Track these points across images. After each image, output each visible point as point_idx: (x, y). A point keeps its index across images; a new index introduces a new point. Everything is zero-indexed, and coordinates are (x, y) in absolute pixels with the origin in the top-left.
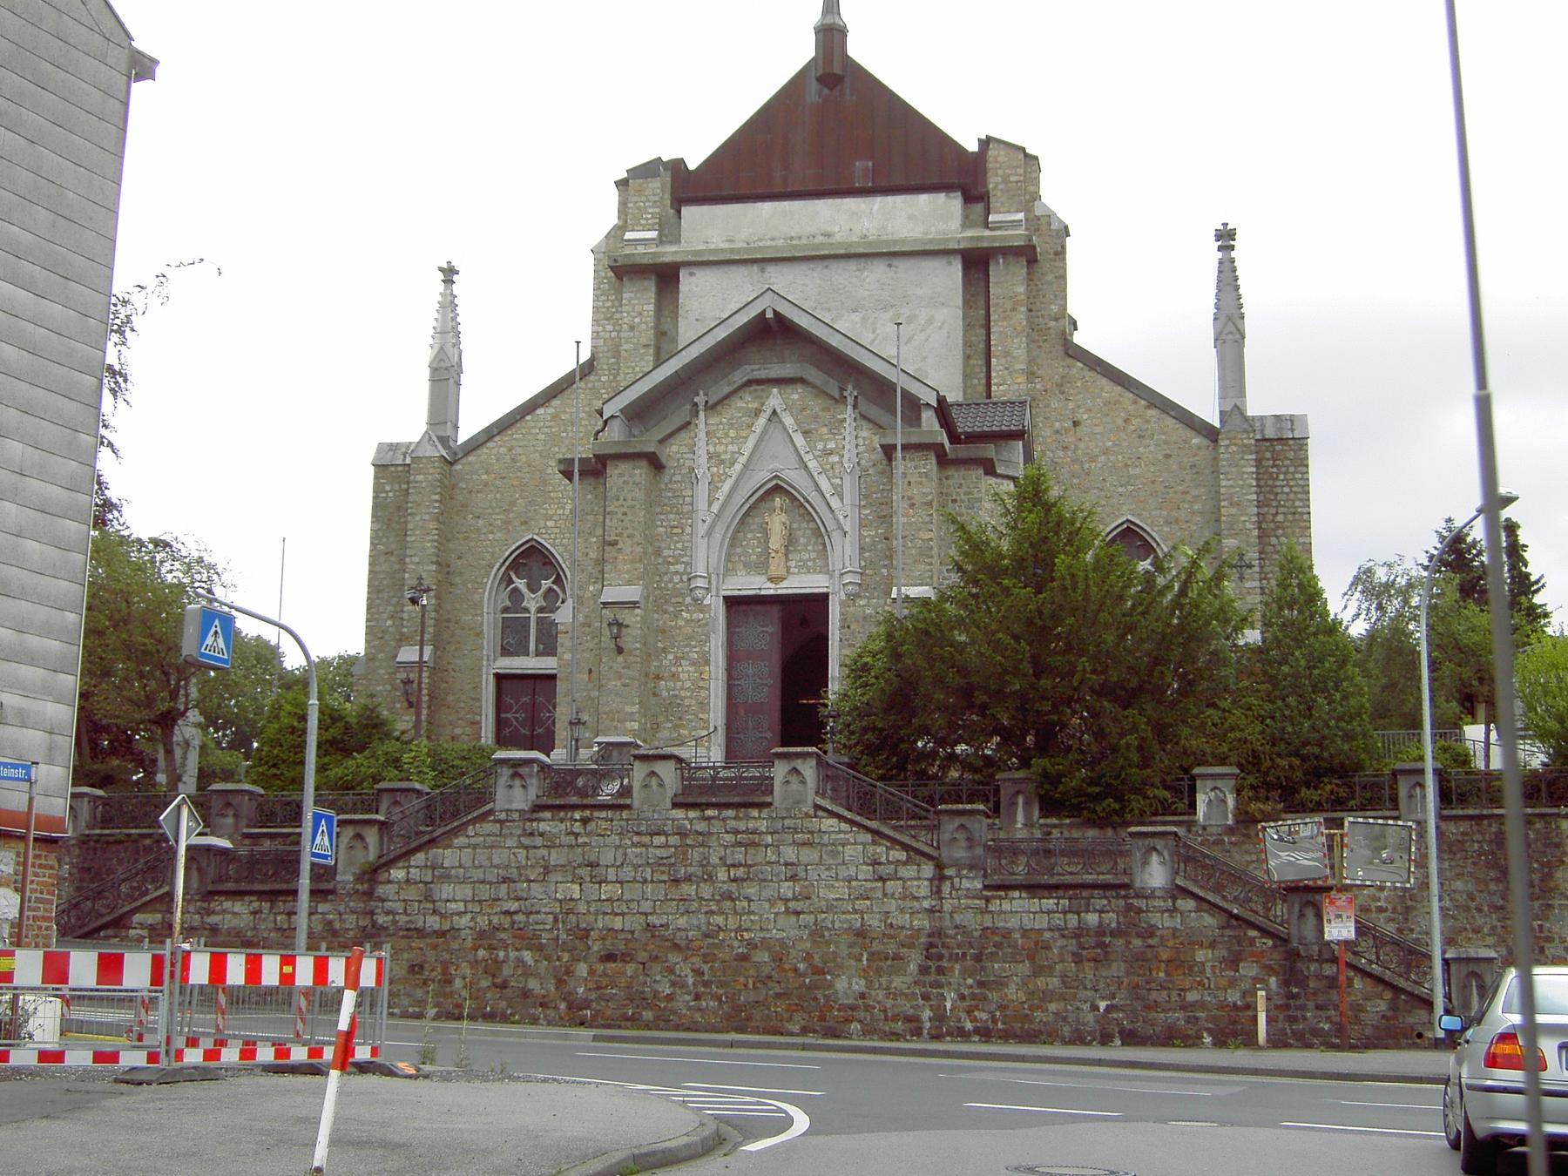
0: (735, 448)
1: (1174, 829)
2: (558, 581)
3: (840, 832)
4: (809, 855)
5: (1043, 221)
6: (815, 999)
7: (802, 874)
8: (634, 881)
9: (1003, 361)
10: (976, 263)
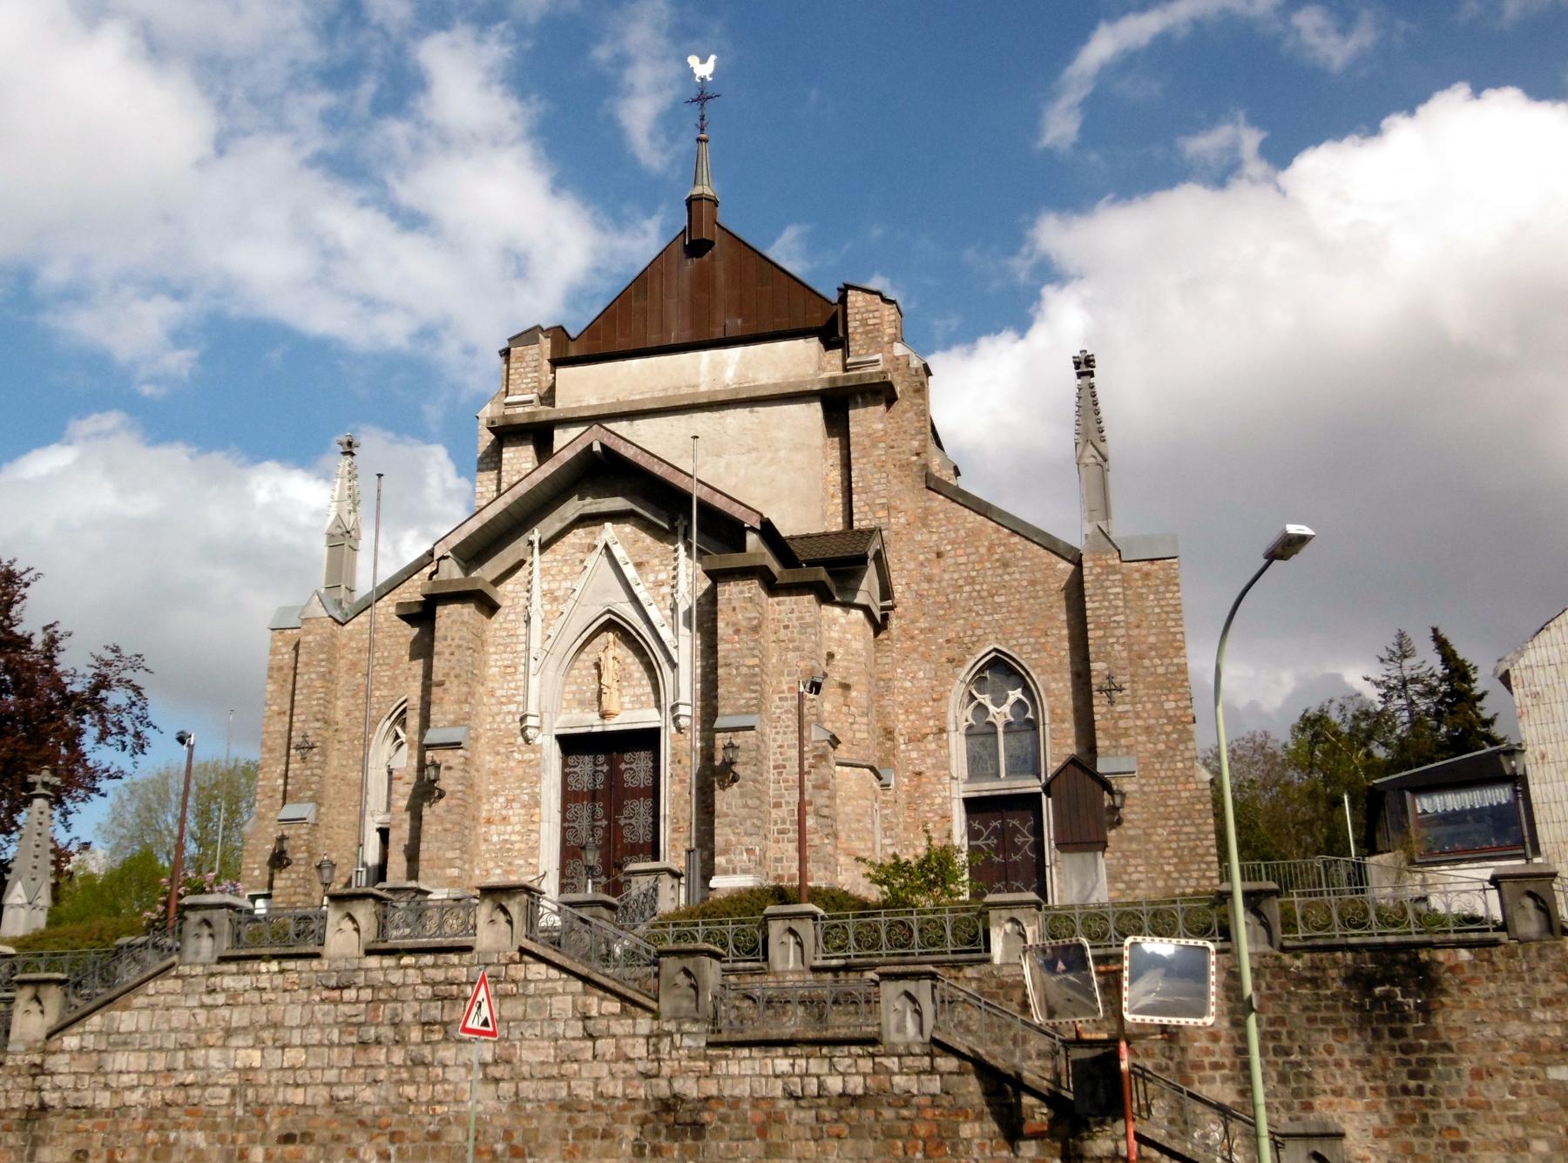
0: (568, 584)
1: (931, 968)
3: (548, 980)
4: (512, 1009)
5: (902, 361)
8: (320, 1045)
9: (864, 496)
10: (837, 404)
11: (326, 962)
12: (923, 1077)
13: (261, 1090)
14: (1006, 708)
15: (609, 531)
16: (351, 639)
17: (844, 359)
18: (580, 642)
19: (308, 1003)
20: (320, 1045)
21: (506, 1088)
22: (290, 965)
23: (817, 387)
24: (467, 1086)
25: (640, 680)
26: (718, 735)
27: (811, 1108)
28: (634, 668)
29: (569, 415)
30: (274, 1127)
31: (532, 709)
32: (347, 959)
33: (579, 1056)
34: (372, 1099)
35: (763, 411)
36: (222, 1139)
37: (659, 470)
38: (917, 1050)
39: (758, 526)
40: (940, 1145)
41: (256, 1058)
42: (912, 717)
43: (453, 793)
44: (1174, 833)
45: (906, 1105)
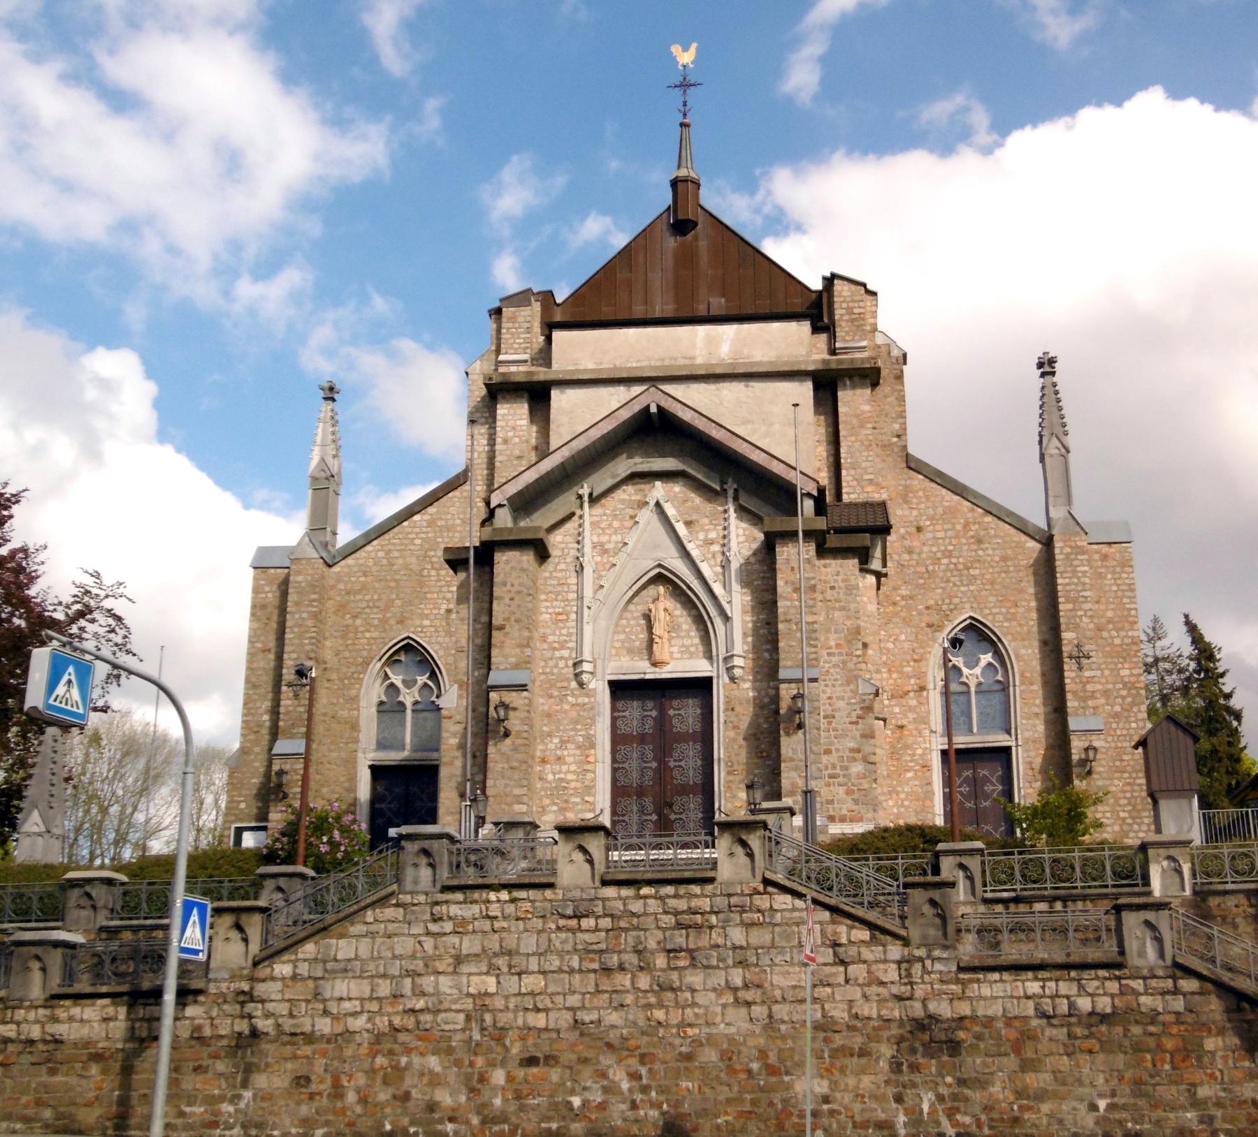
0: (619, 538)
2: (433, 676)
3: (794, 909)
4: (760, 937)
5: (884, 349)
6: (771, 1104)
7: (753, 959)
8: (560, 971)
9: (853, 472)
10: (826, 385)
11: (560, 892)
12: (1168, 997)
13: (499, 1015)
14: (978, 671)
15: (659, 490)
16: (339, 580)
17: (829, 343)
18: (630, 593)
19: (543, 931)
20: (560, 971)
21: (759, 1011)
22: (522, 894)
23: (811, 368)
24: (719, 1009)
25: (688, 631)
26: (782, 686)
27: (1062, 1026)
28: (681, 620)
29: (568, 377)
30: (514, 1051)
31: (587, 655)
32: (582, 890)
33: (831, 981)
34: (620, 1022)
35: (757, 386)
36: (458, 1063)
37: (716, 434)
38: (1160, 973)
39: (815, 493)
40: (1186, 1057)
41: (491, 984)
42: (895, 676)
43: (519, 732)
44: (1129, 784)
45: (1152, 1023)
